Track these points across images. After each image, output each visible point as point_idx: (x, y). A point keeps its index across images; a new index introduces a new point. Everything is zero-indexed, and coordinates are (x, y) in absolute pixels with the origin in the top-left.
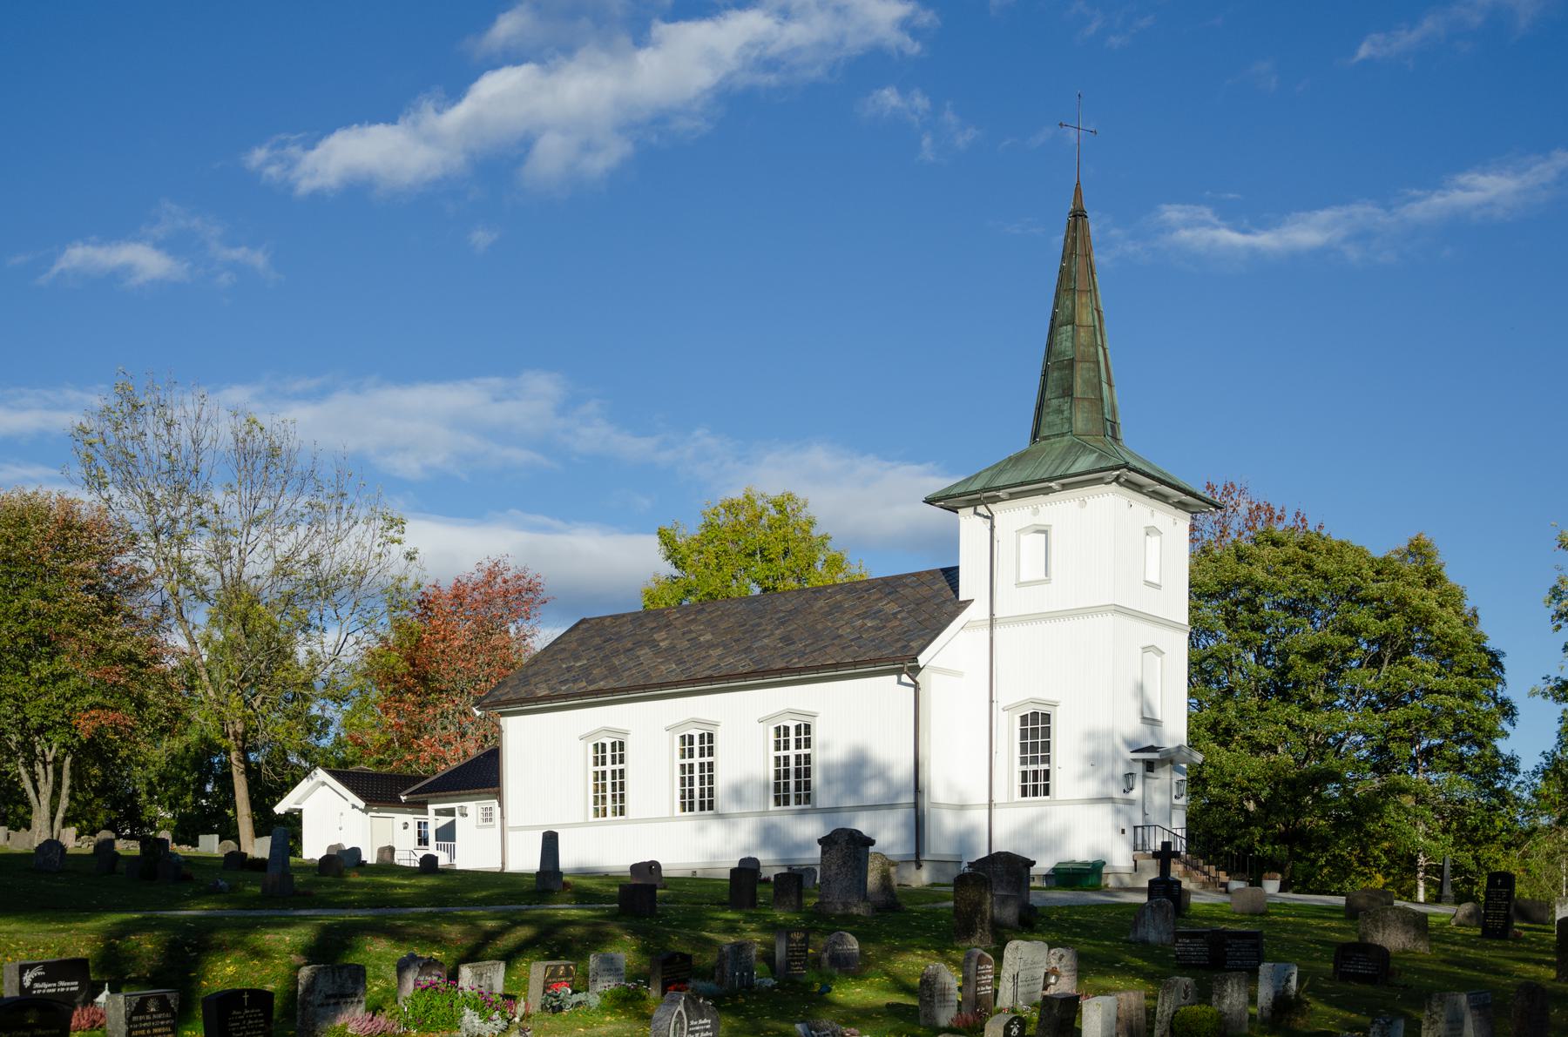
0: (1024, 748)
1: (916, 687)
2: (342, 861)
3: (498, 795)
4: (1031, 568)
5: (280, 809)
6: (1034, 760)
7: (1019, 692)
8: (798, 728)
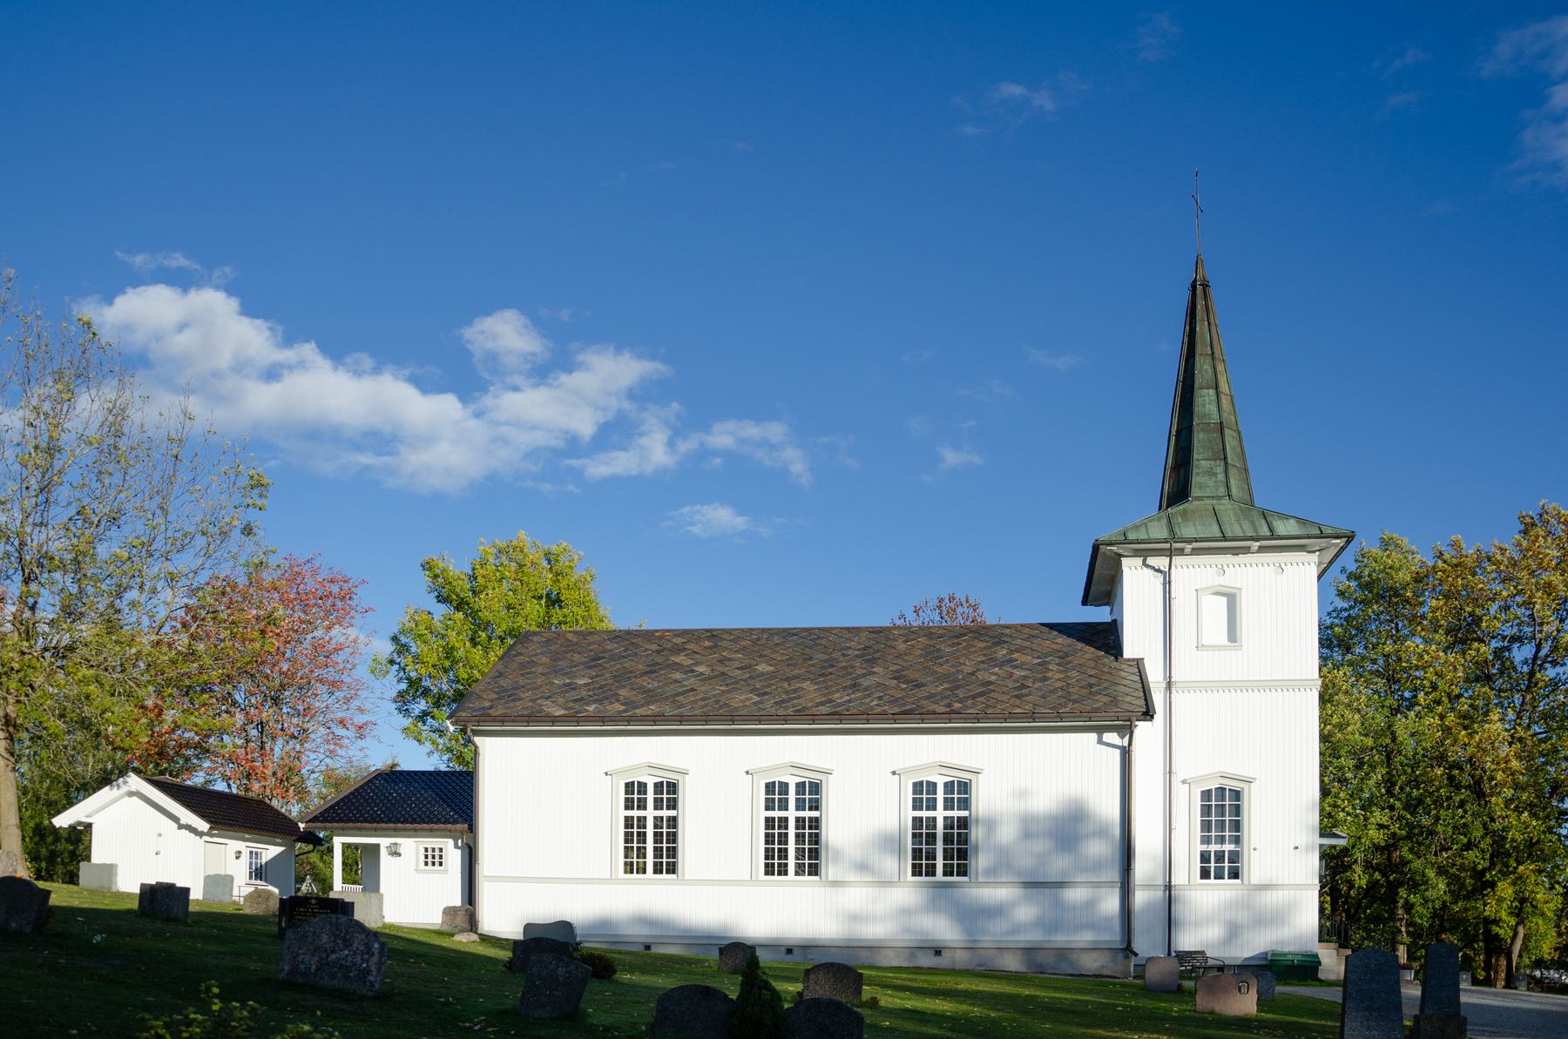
0: (1206, 826)
1: (1126, 754)
2: (162, 900)
4: (1215, 629)
5: (62, 821)
7: (1203, 764)
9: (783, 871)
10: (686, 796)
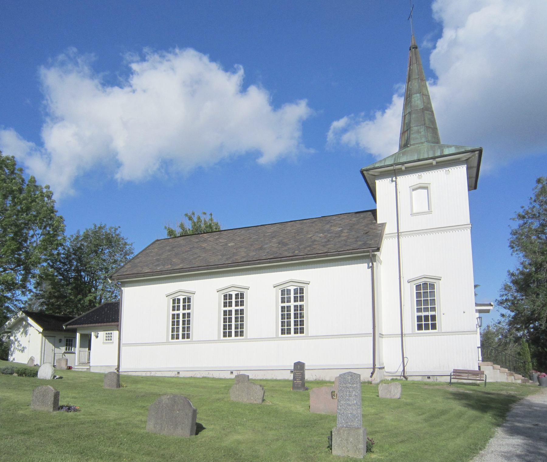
0: (419, 303)
3: (118, 328)
6: (426, 310)
7: (415, 270)
8: (237, 295)
9: (289, 332)
10: (195, 303)
